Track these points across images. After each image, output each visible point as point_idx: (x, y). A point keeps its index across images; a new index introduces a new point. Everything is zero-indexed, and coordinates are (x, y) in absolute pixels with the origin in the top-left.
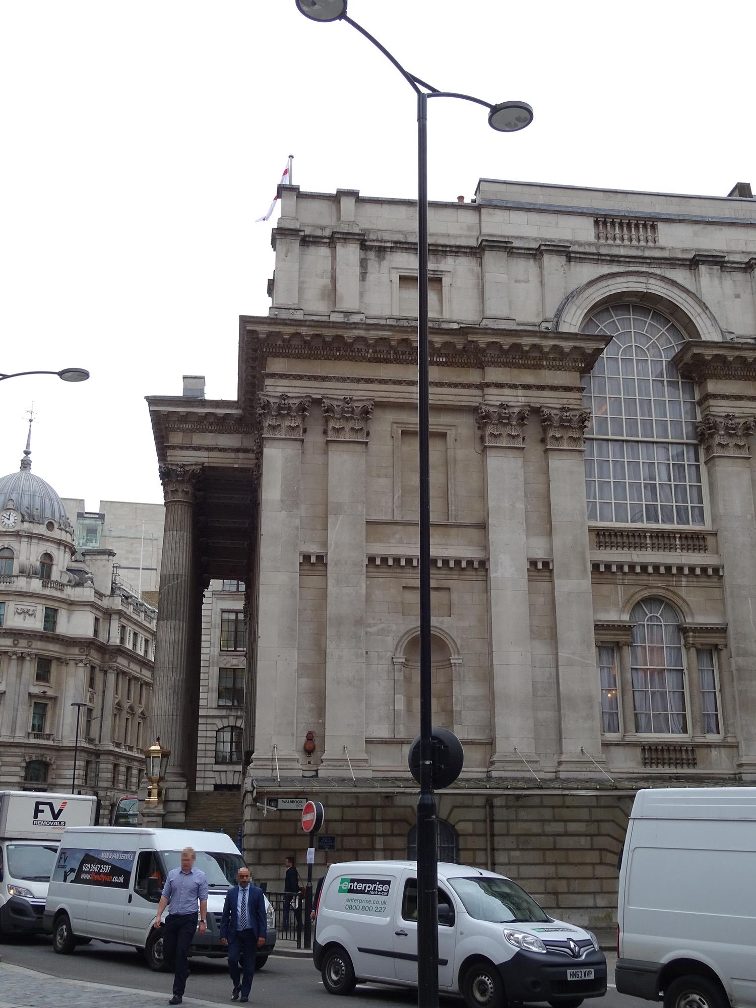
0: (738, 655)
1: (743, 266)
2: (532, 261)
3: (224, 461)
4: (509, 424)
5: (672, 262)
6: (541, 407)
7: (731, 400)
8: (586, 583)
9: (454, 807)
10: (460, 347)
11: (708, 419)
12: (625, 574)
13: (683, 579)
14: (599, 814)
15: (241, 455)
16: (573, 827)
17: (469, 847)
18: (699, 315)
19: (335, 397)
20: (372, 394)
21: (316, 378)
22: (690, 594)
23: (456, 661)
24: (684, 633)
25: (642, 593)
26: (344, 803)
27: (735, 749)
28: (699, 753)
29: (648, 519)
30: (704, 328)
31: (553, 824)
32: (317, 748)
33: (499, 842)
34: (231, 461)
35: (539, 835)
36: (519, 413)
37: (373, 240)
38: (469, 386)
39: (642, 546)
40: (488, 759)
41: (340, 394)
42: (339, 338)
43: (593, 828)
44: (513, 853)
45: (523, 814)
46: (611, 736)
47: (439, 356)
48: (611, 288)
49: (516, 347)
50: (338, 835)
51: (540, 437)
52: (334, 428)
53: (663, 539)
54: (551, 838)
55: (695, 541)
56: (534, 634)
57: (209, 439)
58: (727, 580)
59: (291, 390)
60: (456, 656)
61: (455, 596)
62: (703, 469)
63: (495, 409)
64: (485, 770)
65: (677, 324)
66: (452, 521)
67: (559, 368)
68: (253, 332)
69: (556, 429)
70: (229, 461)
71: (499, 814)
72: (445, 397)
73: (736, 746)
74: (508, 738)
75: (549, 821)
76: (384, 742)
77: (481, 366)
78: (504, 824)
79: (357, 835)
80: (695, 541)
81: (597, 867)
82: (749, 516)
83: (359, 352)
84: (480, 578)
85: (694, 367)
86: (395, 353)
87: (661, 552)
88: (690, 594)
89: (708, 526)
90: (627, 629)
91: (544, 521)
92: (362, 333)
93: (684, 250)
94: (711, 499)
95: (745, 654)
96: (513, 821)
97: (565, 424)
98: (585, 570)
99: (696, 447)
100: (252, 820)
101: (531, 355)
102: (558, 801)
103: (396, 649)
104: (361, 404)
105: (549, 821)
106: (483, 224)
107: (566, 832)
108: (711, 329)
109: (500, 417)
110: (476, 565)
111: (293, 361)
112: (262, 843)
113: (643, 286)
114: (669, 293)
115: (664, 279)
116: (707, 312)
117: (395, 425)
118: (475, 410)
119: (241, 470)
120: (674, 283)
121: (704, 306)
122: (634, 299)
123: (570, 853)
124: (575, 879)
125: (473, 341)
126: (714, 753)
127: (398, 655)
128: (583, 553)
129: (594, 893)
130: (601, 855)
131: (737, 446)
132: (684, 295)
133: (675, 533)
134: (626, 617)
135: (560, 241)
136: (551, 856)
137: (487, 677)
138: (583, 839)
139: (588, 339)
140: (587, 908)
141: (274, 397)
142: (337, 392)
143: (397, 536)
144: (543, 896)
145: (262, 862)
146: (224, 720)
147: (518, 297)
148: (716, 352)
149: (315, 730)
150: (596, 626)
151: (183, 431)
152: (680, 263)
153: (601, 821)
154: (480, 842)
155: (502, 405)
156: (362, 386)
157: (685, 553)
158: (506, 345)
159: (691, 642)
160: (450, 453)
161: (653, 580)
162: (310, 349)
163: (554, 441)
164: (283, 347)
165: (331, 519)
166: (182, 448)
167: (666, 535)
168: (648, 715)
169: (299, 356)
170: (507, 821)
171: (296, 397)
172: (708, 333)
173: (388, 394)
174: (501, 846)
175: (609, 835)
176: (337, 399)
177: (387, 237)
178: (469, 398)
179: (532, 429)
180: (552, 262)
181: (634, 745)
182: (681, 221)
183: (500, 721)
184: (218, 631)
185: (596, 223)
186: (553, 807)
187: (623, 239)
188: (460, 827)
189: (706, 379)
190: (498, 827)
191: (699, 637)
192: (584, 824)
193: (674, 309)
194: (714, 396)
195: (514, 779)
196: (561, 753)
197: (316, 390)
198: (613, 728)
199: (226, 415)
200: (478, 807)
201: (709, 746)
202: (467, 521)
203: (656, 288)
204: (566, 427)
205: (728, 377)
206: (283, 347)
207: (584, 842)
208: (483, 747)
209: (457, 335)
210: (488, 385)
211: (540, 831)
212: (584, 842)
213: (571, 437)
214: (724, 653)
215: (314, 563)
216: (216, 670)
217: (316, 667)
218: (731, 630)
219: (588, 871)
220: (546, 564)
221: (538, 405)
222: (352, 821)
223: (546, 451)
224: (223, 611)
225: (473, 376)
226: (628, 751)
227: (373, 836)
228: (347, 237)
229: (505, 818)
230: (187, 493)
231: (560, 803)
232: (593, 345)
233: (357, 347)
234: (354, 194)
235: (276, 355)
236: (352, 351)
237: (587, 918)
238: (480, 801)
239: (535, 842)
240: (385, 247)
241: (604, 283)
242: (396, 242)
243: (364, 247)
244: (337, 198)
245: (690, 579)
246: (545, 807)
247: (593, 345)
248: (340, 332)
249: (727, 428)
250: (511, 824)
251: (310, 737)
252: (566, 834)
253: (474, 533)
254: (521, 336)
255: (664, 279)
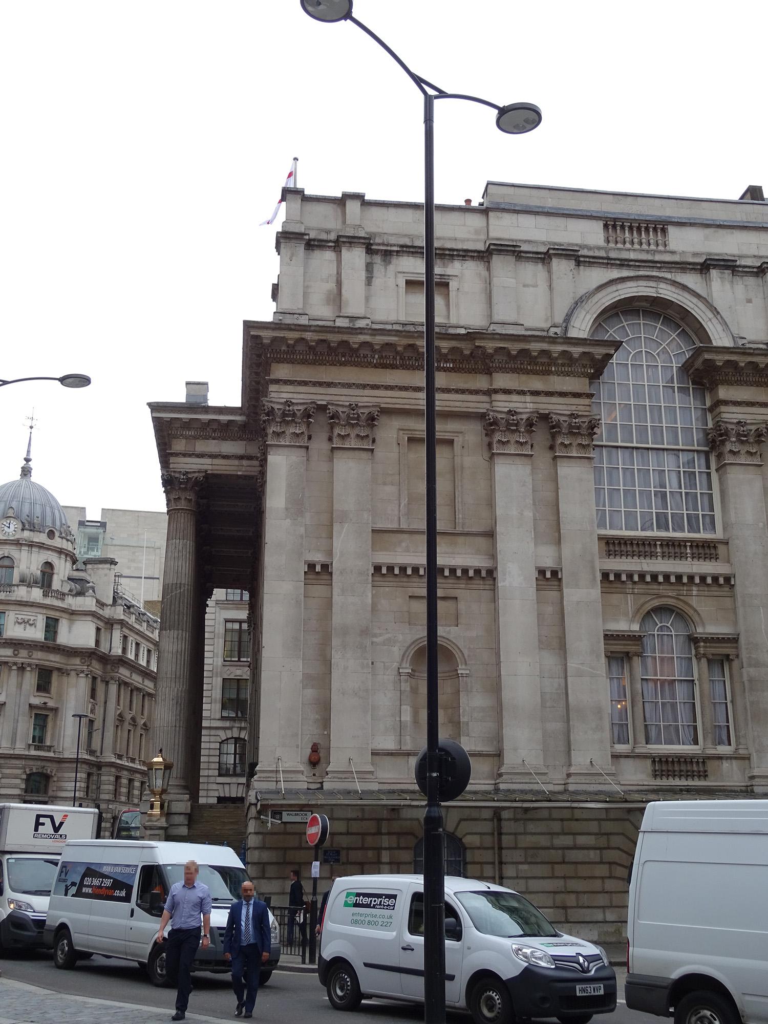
0: (750, 665)
1: (755, 270)
2: (540, 266)
3: (228, 468)
4: (517, 431)
5: (683, 266)
6: (549, 414)
7: (743, 406)
8: (596, 592)
9: (461, 820)
10: (467, 352)
11: (720, 426)
12: (635, 583)
13: (694, 588)
14: (608, 827)
15: (245, 462)
16: (582, 840)
17: (476, 860)
18: (710, 320)
19: (341, 403)
20: (378, 400)
21: (321, 384)
22: (701, 604)
23: (463, 672)
24: (695, 644)
25: (652, 602)
26: (349, 816)
27: (747, 761)
28: (710, 765)
29: (659, 527)
30: (715, 334)
31: (562, 837)
32: (322, 760)
33: (507, 855)
34: (235, 468)
35: (548, 848)
36: (528, 419)
37: (379, 244)
38: (476, 392)
39: (652, 555)
40: (495, 771)
41: (345, 401)
42: (345, 343)
43: (603, 841)
44: (521, 867)
45: (531, 827)
46: (621, 748)
47: (446, 362)
48: (621, 292)
49: (524, 353)
50: (343, 848)
51: (548, 444)
52: (339, 435)
53: (673, 548)
54: (560, 852)
55: (706, 549)
56: (543, 644)
57: (212, 446)
58: (738, 589)
59: (295, 396)
60: (464, 667)
61: (462, 606)
62: (715, 477)
63: (503, 416)
64: (493, 782)
65: (688, 330)
66: (459, 529)
67: (568, 374)
68: (257, 337)
69: (565, 435)
70: (233, 468)
71: (507, 827)
72: (452, 404)
73: (747, 758)
74: (516, 749)
75: (558, 834)
76: (391, 754)
77: (489, 372)
78: (512, 837)
79: (362, 848)
80: (706, 549)
81: (607, 881)
82: (761, 525)
83: (364, 357)
84: (487, 587)
85: (705, 373)
86: (401, 359)
87: (672, 561)
88: (701, 604)
89: (719, 534)
90: (637, 639)
91: (553, 529)
92: (367, 338)
93: (695, 254)
94: (722, 507)
95: (757, 664)
96: (521, 834)
97: (574, 431)
98: (594, 579)
99: (707, 454)
100: (256, 833)
101: (540, 360)
102: (567, 814)
103: (402, 660)
104: (366, 411)
105: (558, 834)
106: (491, 228)
107: (575, 845)
108: (723, 335)
109: (508, 424)
110: (484, 574)
111: (298, 367)
112: (266, 856)
113: (654, 290)
114: (680, 298)
115: (674, 283)
116: (719, 317)
117: (401, 432)
118: (482, 416)
119: (245, 477)
120: (685, 288)
121: (715, 311)
122: (644, 304)
123: (579, 866)
124: (585, 892)
125: (480, 347)
126: (726, 765)
127: (404, 665)
128: (592, 562)
129: (603, 907)
130: (610, 868)
131: (749, 453)
132: (695, 300)
133: (686, 541)
134: (636, 627)
135: (569, 244)
136: (560, 870)
137: (495, 687)
138: (592, 852)
139: (598, 345)
140: (597, 922)
141: (278, 403)
142: (343, 398)
143: (404, 544)
144: (552, 910)
145: (267, 876)
146: (227, 731)
147: (527, 302)
148: (727, 357)
149: (320, 741)
150: (606, 636)
151: (186, 438)
152: (691, 267)
153: (611, 834)
154: (488, 856)
155: (510, 411)
156: (368, 392)
157: (696, 562)
158: (514, 350)
159: (702, 652)
160: (458, 460)
161: (663, 590)
162: (315, 355)
163: (563, 448)
164: (287, 353)
165: (336, 527)
166: (184, 455)
167: (676, 543)
168: (658, 726)
169: (303, 362)
170: (515, 834)
171: (301, 404)
172: (720, 338)
173: (394, 401)
174: (509, 859)
175: (619, 849)
176: (343, 406)
177: (393, 240)
178: (477, 404)
179: (541, 436)
180: (561, 267)
181: (644, 757)
182: (692, 225)
183: (508, 732)
184: (221, 641)
185: (606, 226)
186: (562, 820)
187: (632, 243)
188: (467, 840)
189: (717, 385)
190: (506, 840)
191: (710, 647)
192: (593, 837)
193: (685, 314)
194: (726, 403)
195: (522, 791)
196: (570, 765)
197: (321, 396)
198: (623, 740)
199: (230, 421)
200: (485, 820)
201: (720, 758)
202: (474, 529)
203: (667, 292)
204: (575, 434)
205: (739, 383)
206: (287, 353)
207: (593, 855)
208: (491, 759)
209: (465, 340)
210: (496, 391)
211: (549, 844)
212: (593, 855)
213: (580, 444)
214: (736, 664)
215: (319, 572)
216: (219, 681)
217: (321, 678)
218: (742, 640)
219: (597, 885)
220: (555, 573)
221: (547, 412)
222: (358, 834)
223: (555, 458)
224: (227, 621)
225: (481, 382)
226: (638, 762)
227: (379, 849)
228: (352, 241)
229: (513, 831)
230: (190, 500)
231: (569, 816)
232: (603, 351)
233: (362, 352)
234: (359, 197)
235: (280, 361)
236: (357, 357)
237: (596, 933)
238: (487, 814)
239: (543, 855)
240: (391, 251)
241: (613, 288)
242: (402, 246)
243: (370, 251)
244: (342, 201)
245: (701, 588)
246: (554, 820)
247: (603, 351)
248: (345, 337)
249: (738, 435)
250: (519, 837)
251: (315, 749)
252: (575, 847)
253: (482, 542)
254: (530, 342)
255: (674, 283)
